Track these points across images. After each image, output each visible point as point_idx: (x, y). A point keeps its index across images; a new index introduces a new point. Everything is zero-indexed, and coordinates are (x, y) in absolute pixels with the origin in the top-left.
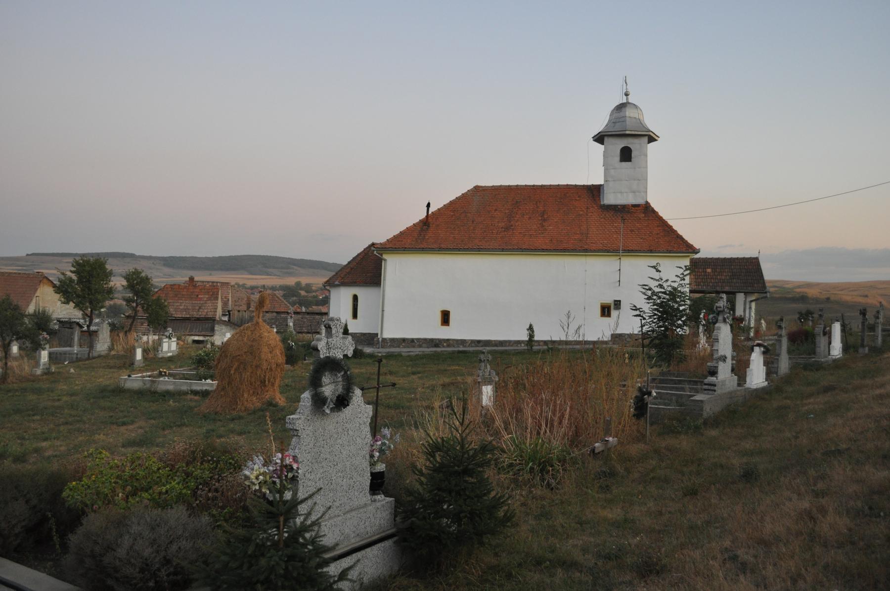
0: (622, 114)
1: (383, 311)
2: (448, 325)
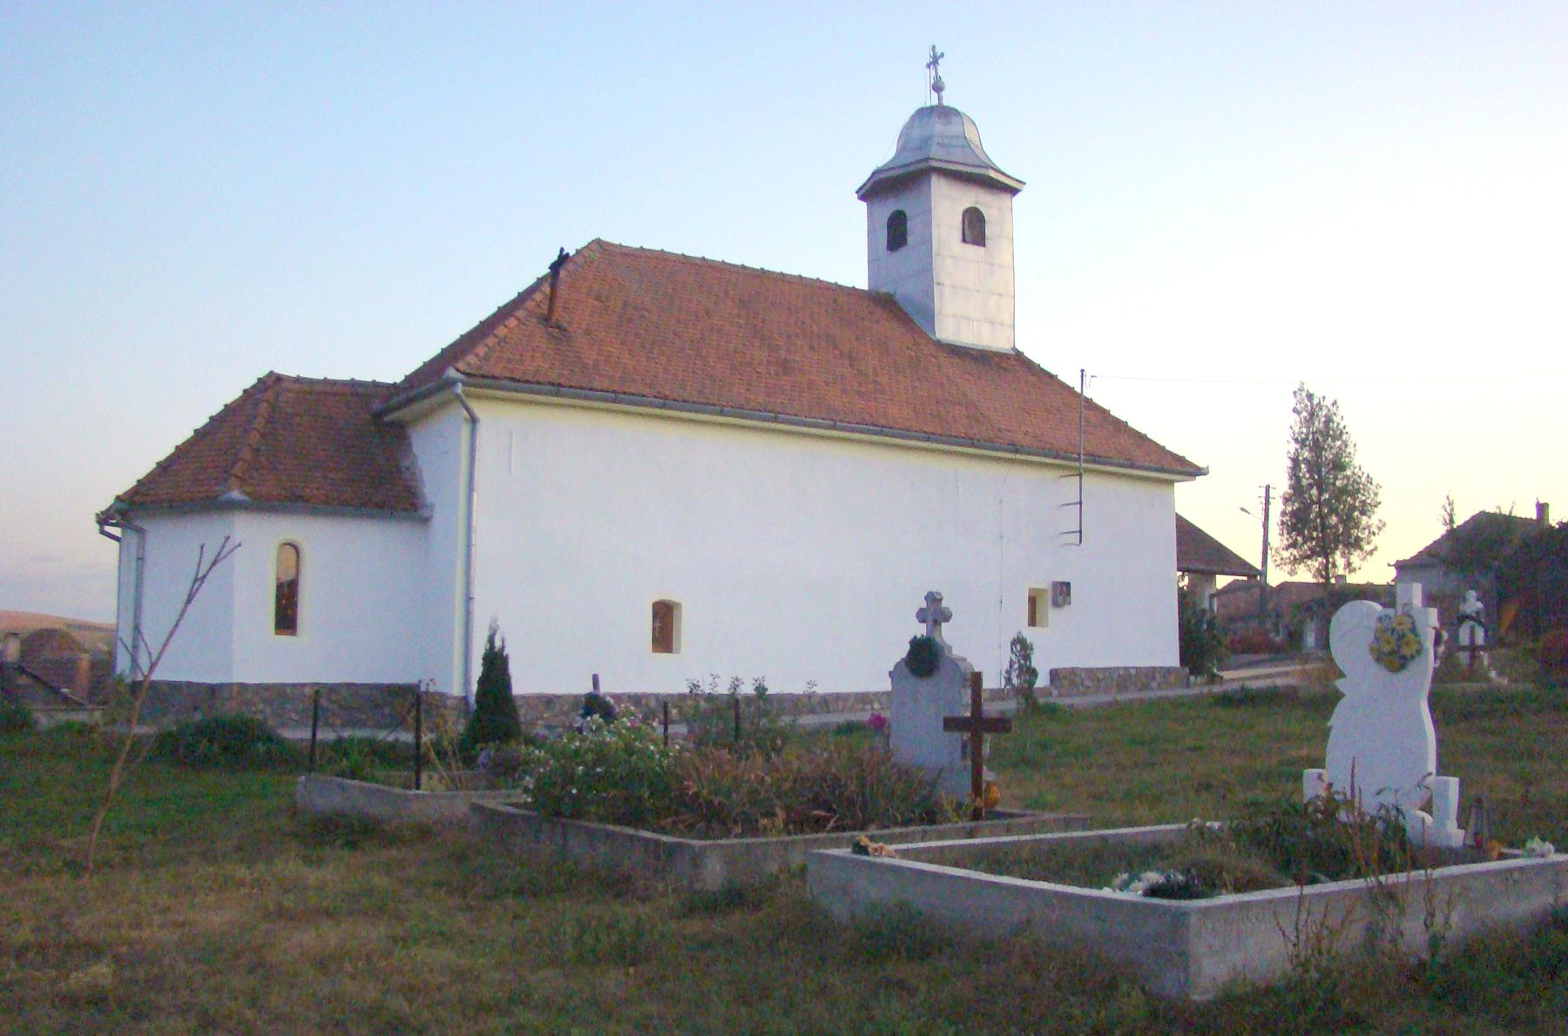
1: (469, 599)
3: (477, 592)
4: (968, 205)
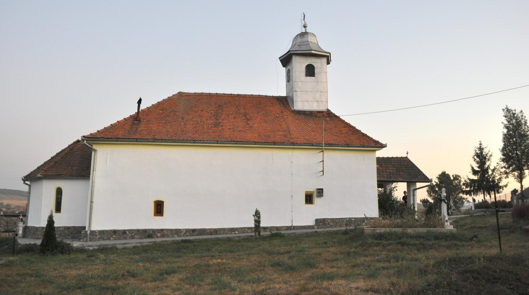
0: (305, 39)
1: (92, 202)
2: (162, 215)
3: (95, 200)
4: (308, 64)
